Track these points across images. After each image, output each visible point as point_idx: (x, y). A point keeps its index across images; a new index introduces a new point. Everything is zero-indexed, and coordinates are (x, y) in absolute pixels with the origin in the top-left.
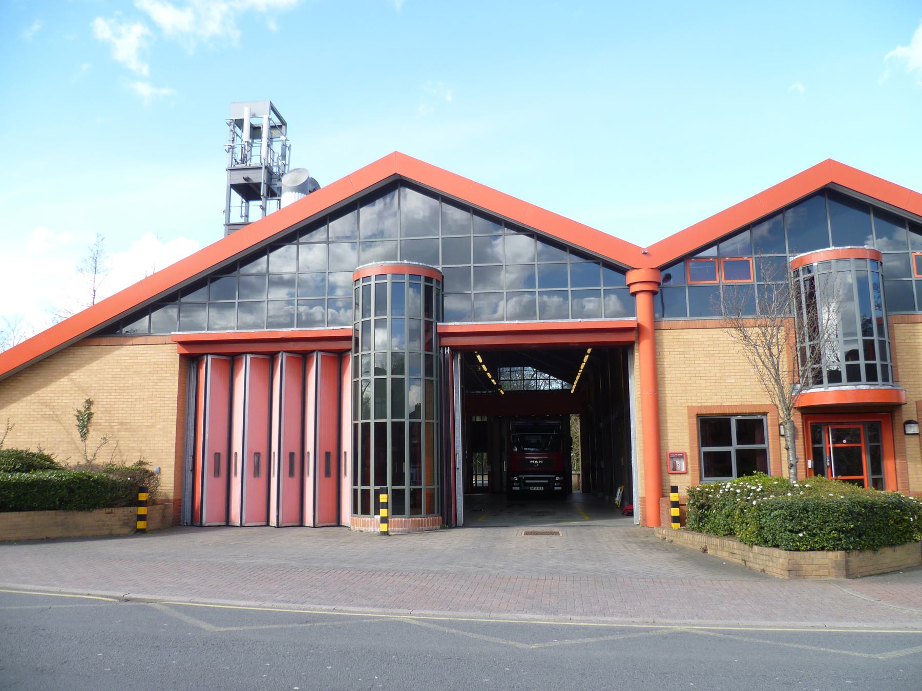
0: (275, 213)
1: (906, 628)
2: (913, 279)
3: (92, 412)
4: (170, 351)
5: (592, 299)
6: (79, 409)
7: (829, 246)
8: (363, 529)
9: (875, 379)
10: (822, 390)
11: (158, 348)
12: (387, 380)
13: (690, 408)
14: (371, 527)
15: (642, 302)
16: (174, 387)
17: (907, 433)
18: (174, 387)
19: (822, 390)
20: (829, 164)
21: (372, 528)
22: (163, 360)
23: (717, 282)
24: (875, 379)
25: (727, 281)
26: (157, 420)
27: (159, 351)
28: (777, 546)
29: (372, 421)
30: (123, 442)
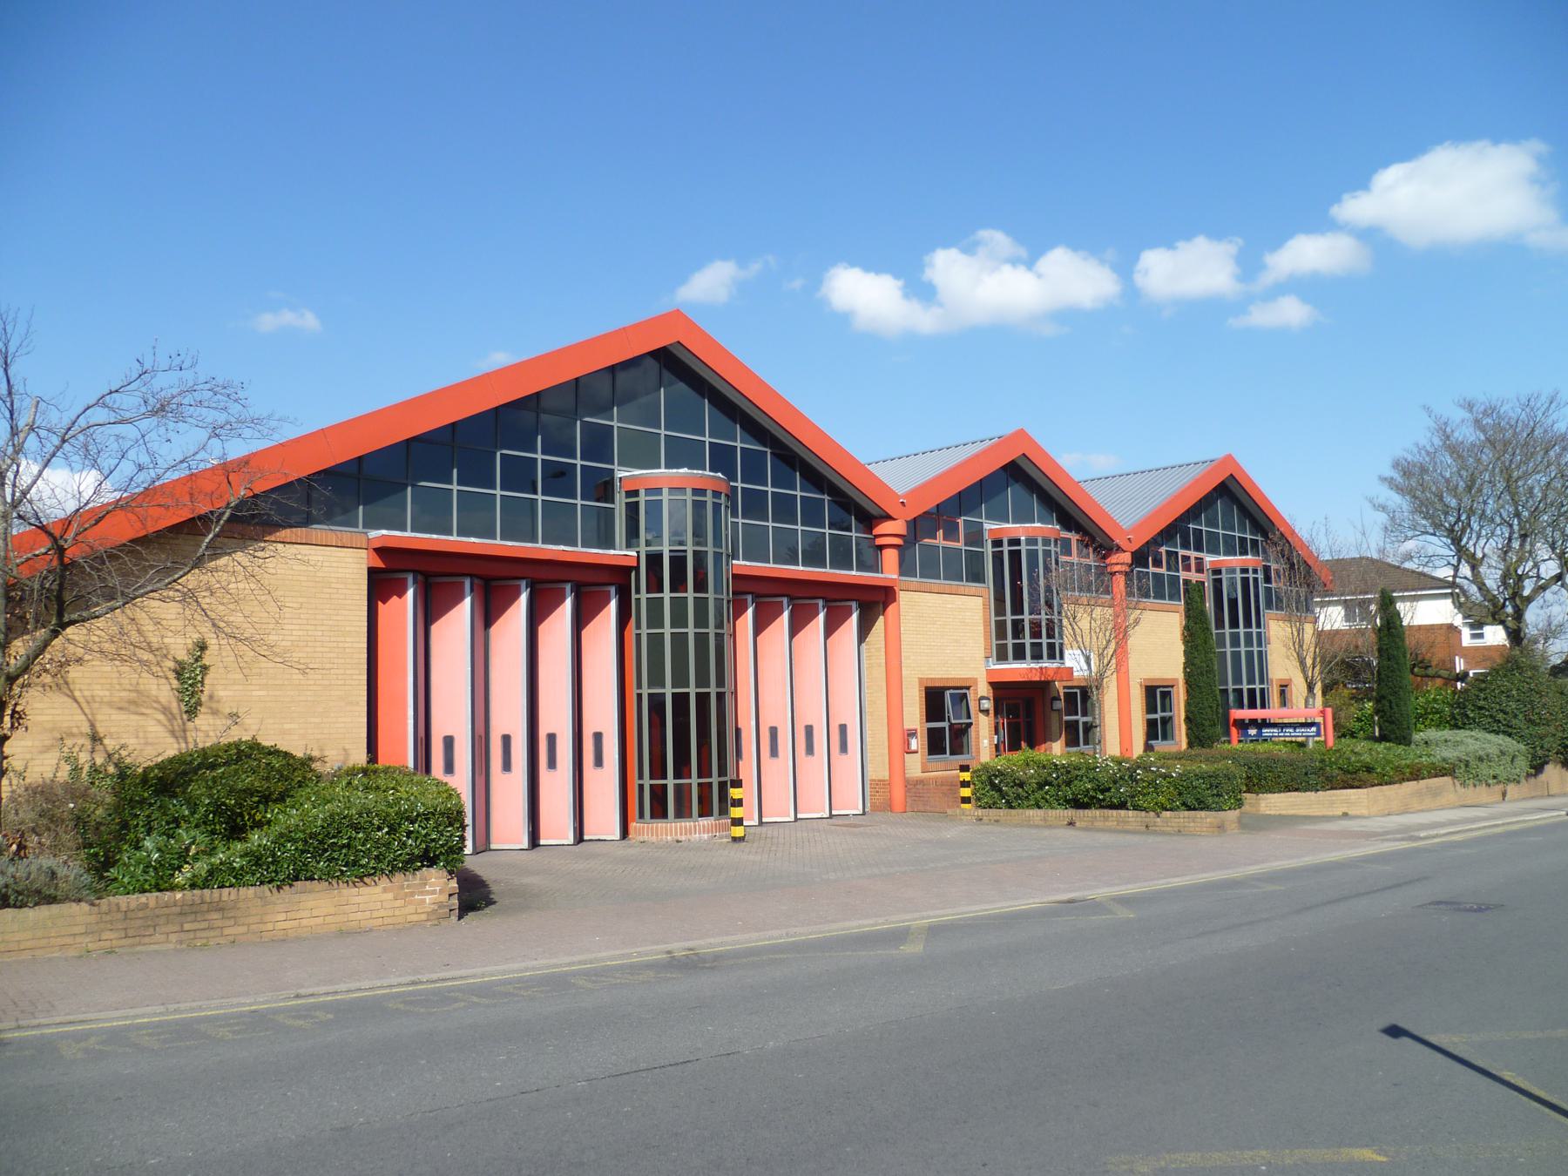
0: (687, 384)
1: (298, 996)
2: (964, 548)
3: (207, 664)
4: (351, 560)
5: (174, 475)
6: (179, 658)
7: (659, 467)
8: (683, 838)
9: (1055, 658)
10: (1024, 666)
11: (328, 553)
12: (689, 634)
13: (921, 680)
14: (695, 833)
15: (890, 557)
16: (359, 624)
17: (1054, 708)
18: (359, 624)
19: (1024, 666)
20: (1021, 435)
21: (697, 835)
22: (340, 575)
23: (938, 541)
24: (1055, 658)
25: (945, 542)
26: (333, 682)
27: (332, 559)
28: (312, 879)
29: (669, 691)
30: (271, 721)
